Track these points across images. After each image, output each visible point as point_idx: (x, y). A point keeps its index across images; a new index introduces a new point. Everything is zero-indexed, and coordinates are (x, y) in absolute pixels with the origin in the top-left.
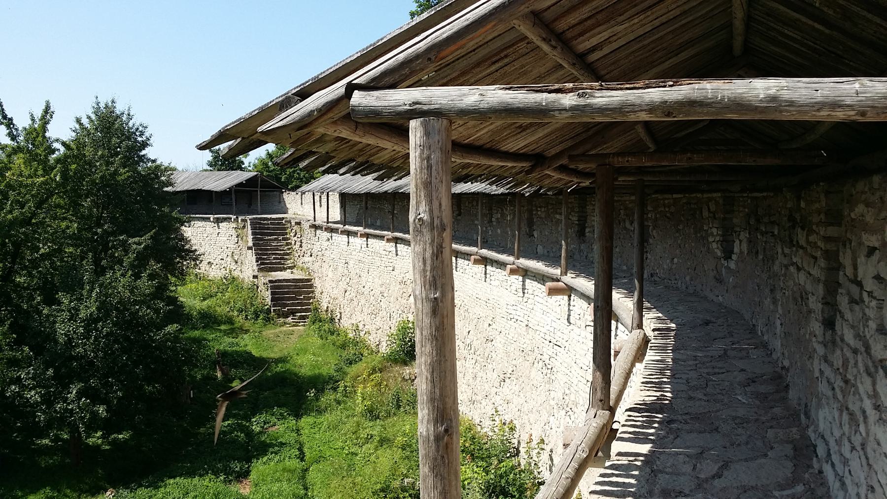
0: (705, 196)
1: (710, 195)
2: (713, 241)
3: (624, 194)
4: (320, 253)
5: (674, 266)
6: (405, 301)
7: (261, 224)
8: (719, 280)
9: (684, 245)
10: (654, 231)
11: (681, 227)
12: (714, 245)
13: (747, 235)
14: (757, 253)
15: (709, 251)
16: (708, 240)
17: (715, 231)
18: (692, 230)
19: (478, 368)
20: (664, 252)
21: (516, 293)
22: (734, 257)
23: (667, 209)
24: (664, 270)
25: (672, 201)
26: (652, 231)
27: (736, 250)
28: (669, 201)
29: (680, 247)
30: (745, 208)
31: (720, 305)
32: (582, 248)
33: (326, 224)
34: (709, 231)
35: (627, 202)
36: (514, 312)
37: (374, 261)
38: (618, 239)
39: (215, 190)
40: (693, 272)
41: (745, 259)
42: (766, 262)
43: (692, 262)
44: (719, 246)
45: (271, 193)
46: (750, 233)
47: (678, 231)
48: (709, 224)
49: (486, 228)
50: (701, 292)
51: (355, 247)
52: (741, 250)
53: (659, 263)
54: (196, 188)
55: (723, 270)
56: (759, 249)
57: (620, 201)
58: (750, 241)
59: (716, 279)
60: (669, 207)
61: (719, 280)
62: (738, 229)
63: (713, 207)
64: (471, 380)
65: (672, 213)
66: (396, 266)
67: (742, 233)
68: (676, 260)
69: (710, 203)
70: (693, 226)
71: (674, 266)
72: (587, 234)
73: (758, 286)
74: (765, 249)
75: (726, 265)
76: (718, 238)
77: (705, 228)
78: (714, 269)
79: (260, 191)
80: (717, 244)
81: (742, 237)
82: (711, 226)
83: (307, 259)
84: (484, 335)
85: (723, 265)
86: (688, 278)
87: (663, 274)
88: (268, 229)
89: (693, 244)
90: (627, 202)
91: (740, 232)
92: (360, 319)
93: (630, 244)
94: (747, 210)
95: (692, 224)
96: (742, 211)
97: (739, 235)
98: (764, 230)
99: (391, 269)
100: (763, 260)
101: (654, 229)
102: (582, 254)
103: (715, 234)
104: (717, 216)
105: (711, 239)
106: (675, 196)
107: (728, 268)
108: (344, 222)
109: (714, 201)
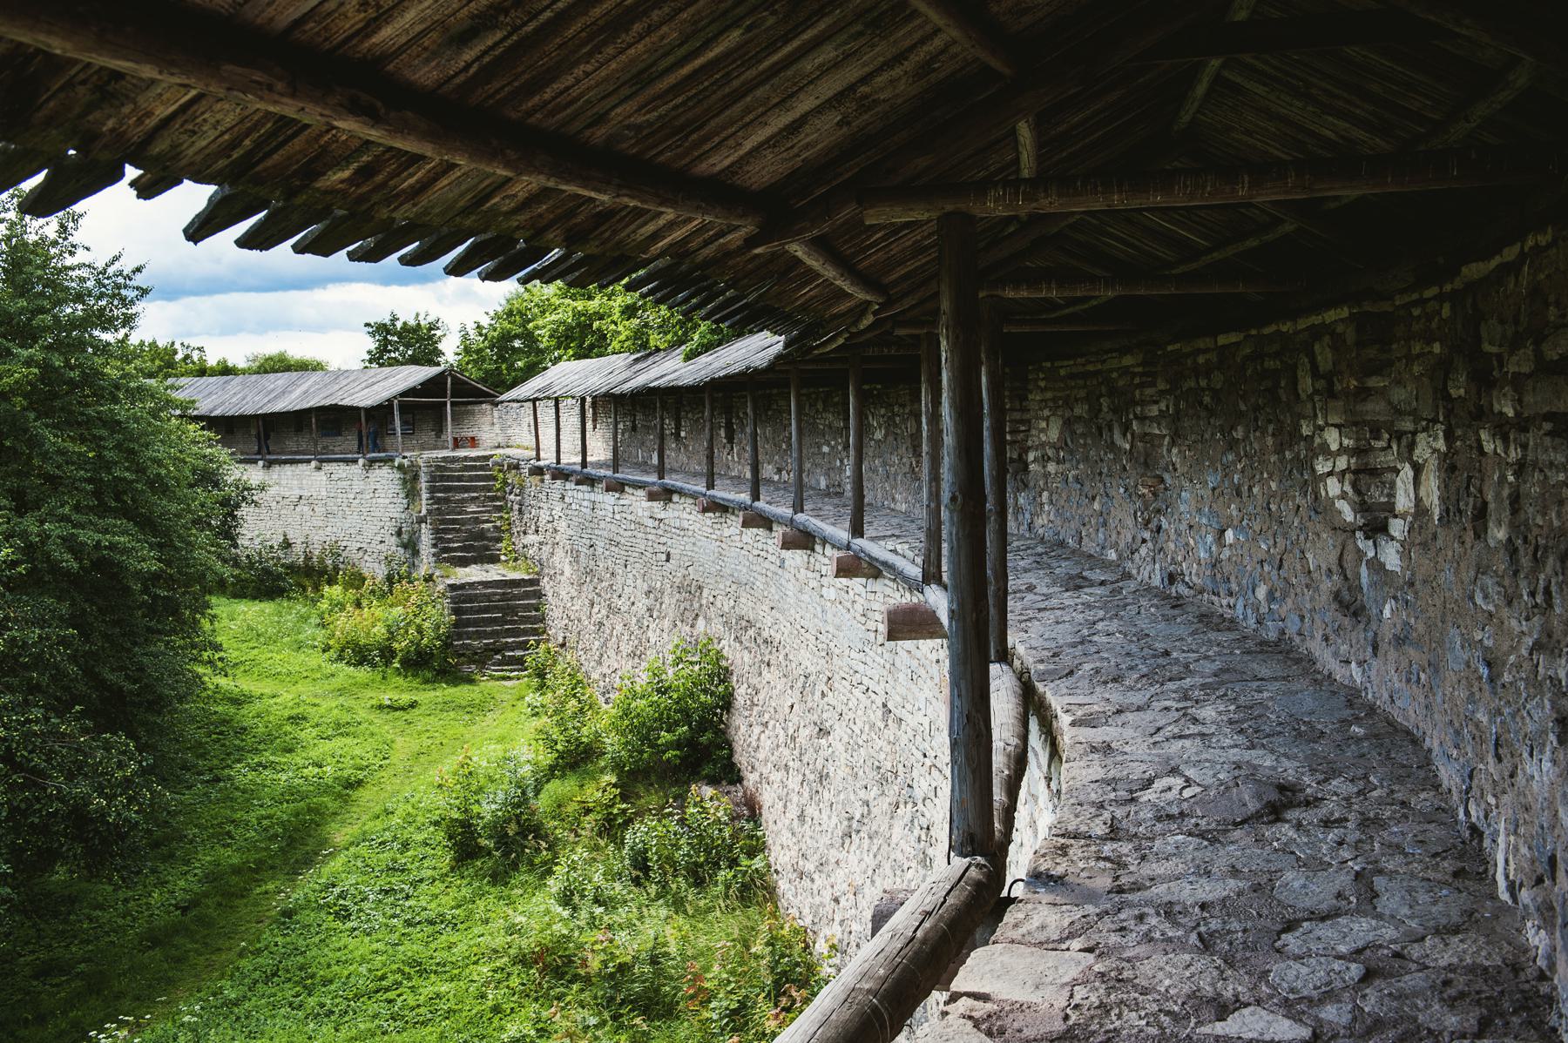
0: (1302, 324)
1: (1315, 320)
2: (1330, 474)
3: (1107, 352)
4: (550, 525)
5: (1226, 553)
6: (688, 629)
7: (446, 469)
8: (1351, 607)
9: (1250, 489)
10: (1175, 451)
11: (1239, 433)
12: (1333, 487)
13: (1441, 445)
14: (1481, 514)
15: (1322, 508)
16: (1313, 470)
17: (1333, 438)
18: (1270, 441)
19: (806, 795)
20: (1199, 510)
21: (863, 620)
22: (1397, 527)
23: (1203, 383)
24: (1199, 564)
25: (1213, 357)
26: (1169, 451)
27: (1404, 502)
28: (1208, 356)
29: (1239, 494)
30: (1429, 342)
31: (1352, 696)
32: (1021, 501)
33: (609, 473)
34: (1317, 440)
35: (1115, 375)
36: (861, 668)
37: (633, 540)
38: (1098, 478)
39: (362, 404)
40: (1275, 572)
41: (1435, 537)
42: (1525, 561)
43: (1271, 542)
44: (1348, 488)
45: (476, 408)
46: (1449, 437)
47: (1232, 445)
48: (1315, 416)
49: (842, 461)
50: (1297, 640)
51: (603, 513)
52: (1418, 500)
53: (1187, 544)
54: (327, 402)
55: (1364, 571)
56: (1490, 497)
57: (1098, 372)
58: (1449, 467)
59: (1340, 602)
60: (1208, 375)
61: (1351, 607)
62: (1408, 425)
63: (1325, 356)
64: (796, 822)
65: (1216, 394)
66: (672, 551)
67: (1421, 438)
68: (1230, 535)
69: (1317, 347)
70: (1271, 428)
71: (1226, 553)
72: (1032, 467)
73: (1489, 664)
74: (1516, 500)
75: (1371, 554)
76: (1342, 463)
77: (1306, 430)
78: (1335, 568)
79: (453, 404)
80: (1341, 481)
81: (1422, 452)
82: (1320, 422)
83: (531, 538)
84: (815, 718)
85: (1360, 554)
86: (1262, 592)
87: (1197, 575)
88: (460, 479)
89: (1273, 485)
90: (1115, 375)
91: (1414, 433)
92: (616, 666)
93: (1122, 490)
94: (1437, 348)
95: (1270, 421)
96: (1418, 356)
97: (1412, 446)
98: (1511, 414)
99: (664, 557)
100: (1511, 549)
101: (1173, 443)
102: (1020, 518)
103: (1334, 447)
104: (1338, 387)
105: (1322, 467)
106: (1222, 340)
107: (1377, 566)
108: (615, 464)
109: (1327, 339)
